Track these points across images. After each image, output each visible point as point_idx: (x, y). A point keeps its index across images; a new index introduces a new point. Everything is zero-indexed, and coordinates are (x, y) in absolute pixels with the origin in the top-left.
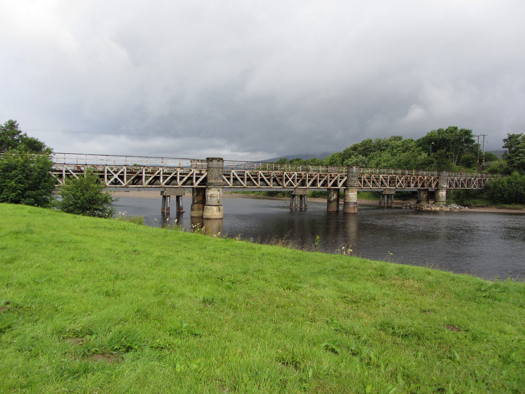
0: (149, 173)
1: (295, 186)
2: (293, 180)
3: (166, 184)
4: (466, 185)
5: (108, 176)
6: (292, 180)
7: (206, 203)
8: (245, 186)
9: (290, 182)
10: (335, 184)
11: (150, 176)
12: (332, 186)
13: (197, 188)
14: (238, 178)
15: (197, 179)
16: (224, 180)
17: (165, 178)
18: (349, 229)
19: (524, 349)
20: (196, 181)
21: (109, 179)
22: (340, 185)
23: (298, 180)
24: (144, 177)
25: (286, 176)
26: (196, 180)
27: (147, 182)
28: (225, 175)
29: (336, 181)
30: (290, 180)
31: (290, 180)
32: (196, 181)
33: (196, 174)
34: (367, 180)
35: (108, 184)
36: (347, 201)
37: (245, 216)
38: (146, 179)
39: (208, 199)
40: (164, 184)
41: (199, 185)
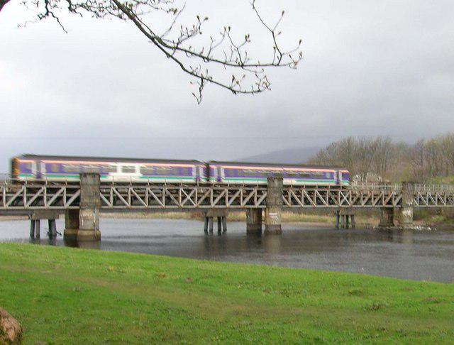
2: (192, 198)
3: (32, 205)
4: (444, 202)
5: (6, 197)
7: (80, 227)
9: (189, 201)
10: (390, 203)
11: (11, 197)
14: (155, 196)
18: (208, 260)
19: (19, 336)
22: (395, 203)
26: (67, 200)
28: (103, 193)
29: (252, 198)
34: (432, 198)
35: (182, 206)
36: (268, 223)
38: (29, 198)
39: (82, 222)
40: (28, 205)
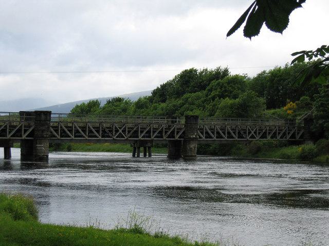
0: (155, 129)
1: (126, 138)
2: (255, 133)
6: (255, 133)
8: (59, 137)
12: (290, 138)
13: (25, 140)
15: (25, 131)
16: (51, 132)
17: (129, 132)
20: (24, 133)
21: (249, 134)
23: (259, 133)
24: (23, 130)
25: (249, 130)
27: (178, 136)
30: (253, 133)
31: (253, 133)
32: (24, 133)
33: (165, 129)
37: (160, 189)
41: (27, 137)
